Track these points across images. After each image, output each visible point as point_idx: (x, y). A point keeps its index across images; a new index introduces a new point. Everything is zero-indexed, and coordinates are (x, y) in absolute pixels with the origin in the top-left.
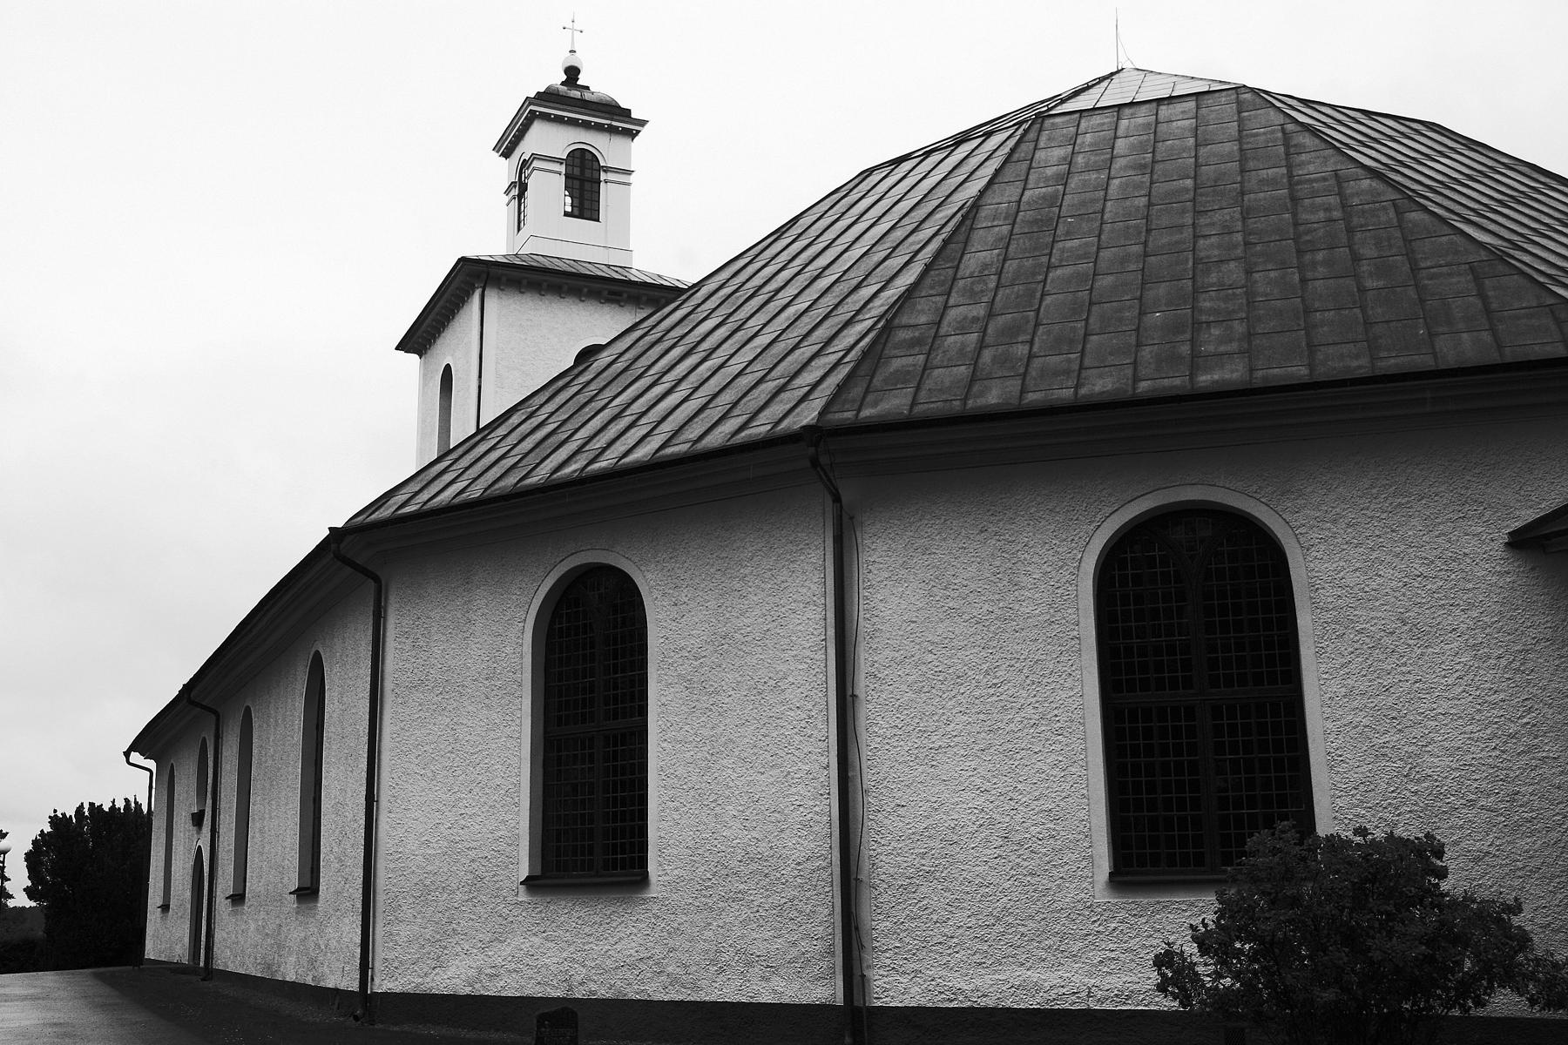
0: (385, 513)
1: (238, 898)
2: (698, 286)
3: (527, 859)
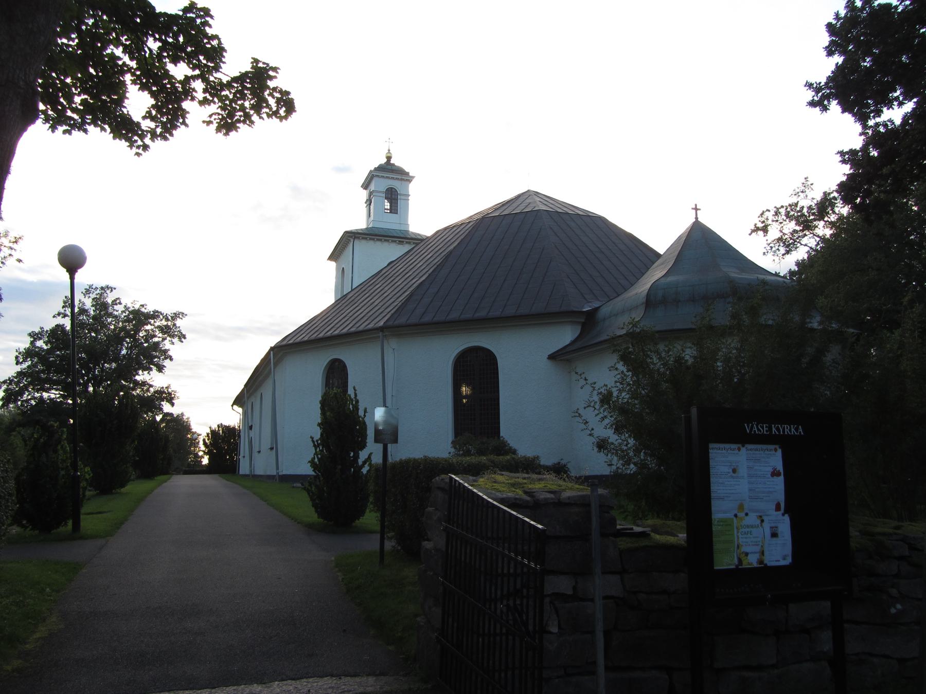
0: (284, 343)
1: (259, 452)
3: (368, 432)
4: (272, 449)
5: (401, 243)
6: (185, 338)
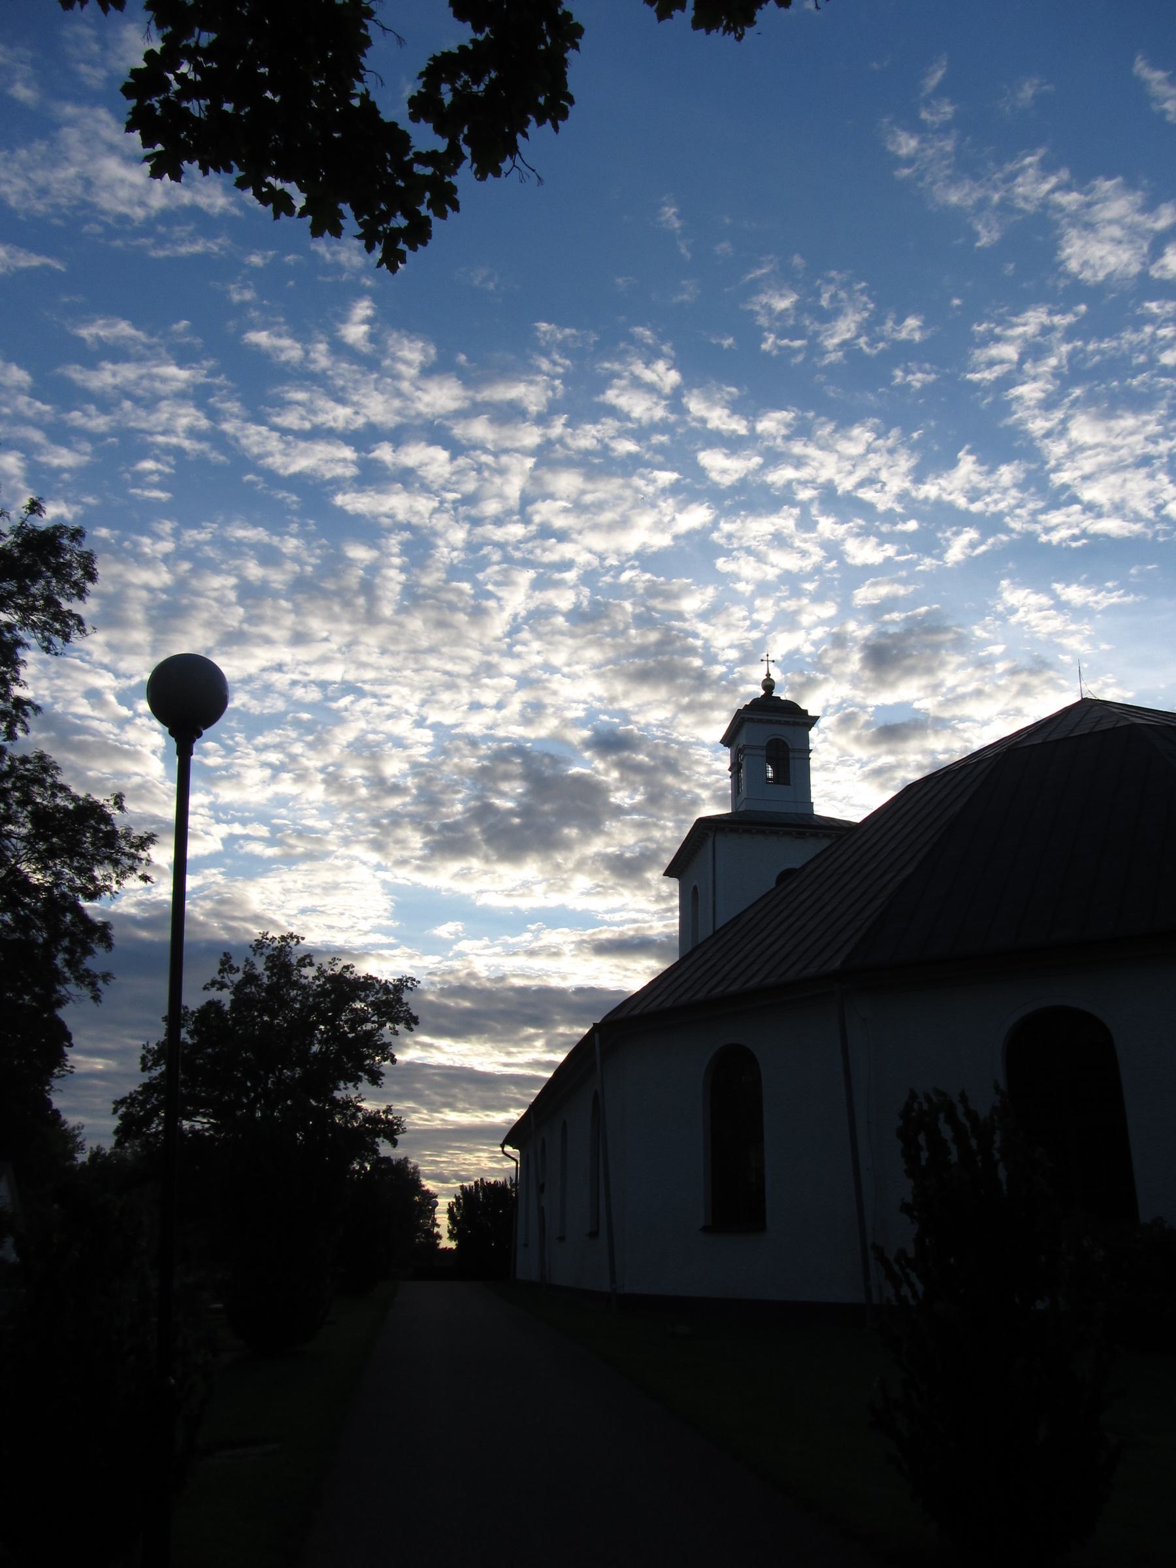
2: (804, 867)
4: (594, 1234)
5: (801, 835)
6: (416, 1023)
